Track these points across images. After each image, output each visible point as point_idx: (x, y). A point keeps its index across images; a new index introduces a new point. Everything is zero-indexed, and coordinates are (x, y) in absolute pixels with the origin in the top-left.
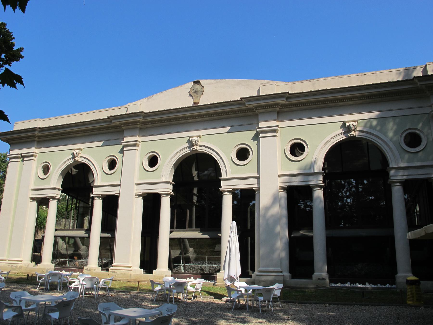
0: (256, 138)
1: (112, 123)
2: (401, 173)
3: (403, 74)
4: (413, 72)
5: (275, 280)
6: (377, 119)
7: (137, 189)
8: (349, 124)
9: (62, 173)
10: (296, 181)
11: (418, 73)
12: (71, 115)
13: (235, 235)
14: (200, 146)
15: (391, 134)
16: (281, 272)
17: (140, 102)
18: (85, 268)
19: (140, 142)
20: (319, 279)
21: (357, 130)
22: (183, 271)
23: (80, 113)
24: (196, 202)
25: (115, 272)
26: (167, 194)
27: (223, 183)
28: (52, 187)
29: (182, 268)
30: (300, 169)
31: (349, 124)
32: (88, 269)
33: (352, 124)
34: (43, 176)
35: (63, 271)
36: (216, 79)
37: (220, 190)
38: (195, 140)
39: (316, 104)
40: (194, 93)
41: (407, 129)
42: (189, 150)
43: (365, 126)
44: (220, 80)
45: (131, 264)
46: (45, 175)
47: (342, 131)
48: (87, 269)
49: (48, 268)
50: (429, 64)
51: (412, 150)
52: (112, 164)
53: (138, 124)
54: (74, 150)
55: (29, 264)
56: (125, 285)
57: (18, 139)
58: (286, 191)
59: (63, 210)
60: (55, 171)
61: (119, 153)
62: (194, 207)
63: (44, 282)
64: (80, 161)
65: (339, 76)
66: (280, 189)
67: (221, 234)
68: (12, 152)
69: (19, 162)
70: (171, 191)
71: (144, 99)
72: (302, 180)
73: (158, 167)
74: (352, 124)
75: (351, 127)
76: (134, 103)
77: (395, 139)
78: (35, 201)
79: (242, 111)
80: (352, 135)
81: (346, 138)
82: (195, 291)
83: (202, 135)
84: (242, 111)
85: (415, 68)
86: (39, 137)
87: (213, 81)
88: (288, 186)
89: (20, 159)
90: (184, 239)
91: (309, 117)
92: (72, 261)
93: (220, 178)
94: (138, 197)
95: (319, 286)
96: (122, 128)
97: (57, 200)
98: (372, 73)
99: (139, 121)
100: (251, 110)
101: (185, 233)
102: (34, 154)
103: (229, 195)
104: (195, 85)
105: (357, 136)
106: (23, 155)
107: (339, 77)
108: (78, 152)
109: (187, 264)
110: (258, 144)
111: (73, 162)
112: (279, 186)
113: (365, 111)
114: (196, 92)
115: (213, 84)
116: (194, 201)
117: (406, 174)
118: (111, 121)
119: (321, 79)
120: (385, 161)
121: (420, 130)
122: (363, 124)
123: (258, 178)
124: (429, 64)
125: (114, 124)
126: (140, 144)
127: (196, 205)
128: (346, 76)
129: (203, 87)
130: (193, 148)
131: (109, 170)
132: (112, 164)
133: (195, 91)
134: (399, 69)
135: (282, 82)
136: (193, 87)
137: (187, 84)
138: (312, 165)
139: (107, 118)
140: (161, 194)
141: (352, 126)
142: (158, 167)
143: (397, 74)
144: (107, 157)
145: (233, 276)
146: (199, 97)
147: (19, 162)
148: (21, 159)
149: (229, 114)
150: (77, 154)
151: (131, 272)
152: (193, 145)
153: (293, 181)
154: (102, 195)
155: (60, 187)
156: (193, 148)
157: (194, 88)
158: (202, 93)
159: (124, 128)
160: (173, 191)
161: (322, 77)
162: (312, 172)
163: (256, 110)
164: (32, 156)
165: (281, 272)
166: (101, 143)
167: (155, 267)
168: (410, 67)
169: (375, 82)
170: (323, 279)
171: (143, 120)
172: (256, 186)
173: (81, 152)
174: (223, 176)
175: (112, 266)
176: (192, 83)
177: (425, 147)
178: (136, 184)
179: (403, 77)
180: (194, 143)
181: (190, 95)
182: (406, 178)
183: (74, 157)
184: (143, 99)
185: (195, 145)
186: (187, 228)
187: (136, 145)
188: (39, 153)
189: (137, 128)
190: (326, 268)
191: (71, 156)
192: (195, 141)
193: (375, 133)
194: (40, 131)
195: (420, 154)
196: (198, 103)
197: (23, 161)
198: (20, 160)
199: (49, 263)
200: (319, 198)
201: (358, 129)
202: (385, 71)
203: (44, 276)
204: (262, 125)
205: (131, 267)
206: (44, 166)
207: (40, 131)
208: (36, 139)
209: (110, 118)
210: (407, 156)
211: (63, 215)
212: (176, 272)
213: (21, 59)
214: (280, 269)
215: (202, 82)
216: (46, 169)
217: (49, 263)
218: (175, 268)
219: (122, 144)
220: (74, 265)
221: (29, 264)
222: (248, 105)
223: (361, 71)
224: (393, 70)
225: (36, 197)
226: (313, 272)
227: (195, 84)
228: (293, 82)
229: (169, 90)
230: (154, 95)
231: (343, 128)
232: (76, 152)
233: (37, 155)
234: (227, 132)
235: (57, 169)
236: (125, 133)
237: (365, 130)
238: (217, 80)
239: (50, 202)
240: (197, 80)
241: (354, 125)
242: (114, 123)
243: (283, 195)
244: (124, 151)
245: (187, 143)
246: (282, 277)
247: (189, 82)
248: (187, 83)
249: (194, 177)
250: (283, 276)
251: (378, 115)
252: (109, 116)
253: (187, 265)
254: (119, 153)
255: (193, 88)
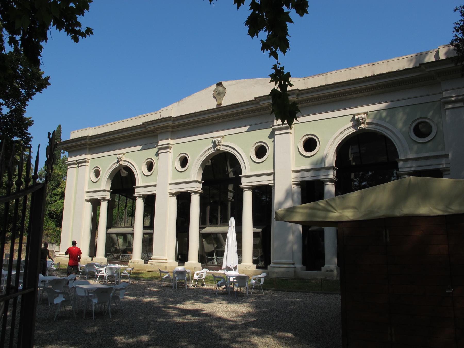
0: (272, 136)
1: (147, 128)
2: (409, 164)
3: (414, 61)
4: (425, 57)
5: (286, 271)
6: (386, 110)
7: (170, 189)
8: (358, 117)
9: (110, 176)
10: (308, 176)
11: (431, 58)
12: (115, 122)
13: (233, 229)
14: (124, 161)
15: (400, 125)
16: (293, 264)
17: (171, 107)
18: (130, 261)
19: (172, 145)
20: (327, 271)
21: (366, 122)
22: (216, 263)
23: (123, 120)
24: (232, 198)
25: (153, 264)
26: (196, 193)
27: (243, 180)
28: (102, 189)
29: (215, 261)
30: (312, 164)
31: (358, 117)
32: (133, 262)
33: (361, 117)
34: (180, 169)
35: (117, 264)
36: (236, 79)
37: (240, 187)
38: (218, 141)
39: (331, 97)
40: (219, 95)
41: (416, 118)
42: (214, 150)
43: (374, 118)
44: (240, 80)
45: (166, 257)
46: (97, 178)
47: (353, 124)
48: (131, 262)
49: (102, 261)
50: (441, 47)
51: (421, 140)
52: (150, 166)
53: (169, 128)
54: (118, 154)
55: (87, 258)
56: (149, 276)
57: (115, 140)
58: (299, 186)
59: (129, 209)
60: (104, 175)
61: (155, 155)
62: (230, 203)
63: (84, 272)
64: (124, 164)
65: (350, 68)
66: (293, 184)
67: (153, 231)
68: (70, 159)
69: (76, 167)
70: (201, 190)
71: (175, 103)
72: (313, 175)
73: (318, 151)
74: (361, 117)
75: (360, 120)
76: (166, 108)
77: (404, 129)
78: (141, 198)
79: (248, 112)
80: (361, 128)
81: (356, 131)
82: (198, 279)
83: (225, 135)
84: (248, 112)
85: (428, 52)
86: (90, 144)
87: (233, 82)
88: (301, 181)
89: (76, 165)
90: (218, 234)
91: (322, 112)
92: (126, 255)
93: (240, 176)
94: (171, 196)
95: (327, 277)
96: (156, 132)
97: (107, 201)
98: (383, 61)
99: (170, 125)
100: (153, 131)
101: (216, 228)
102: (86, 160)
103: (248, 191)
104: (217, 87)
105: (366, 129)
106: (78, 161)
107: (350, 68)
108: (220, 140)
109: (256, 259)
110: (274, 141)
111: (118, 166)
112: (292, 182)
113: (380, 102)
114: (219, 94)
115: (234, 85)
116: (229, 197)
117: (414, 165)
118: (146, 127)
119: (333, 72)
120: (396, 153)
121: (430, 119)
122: (372, 116)
123: (273, 174)
124: (441, 47)
125: (262, 105)
126: (172, 146)
127: (231, 202)
128: (358, 67)
129: (225, 88)
130: (216, 148)
131: (181, 168)
132: (150, 166)
133: (218, 93)
134: (411, 55)
135: (296, 78)
136: (216, 90)
137: (211, 86)
138: (323, 160)
139: (142, 124)
140: (191, 192)
141: (360, 118)
142: (266, 158)
143: (408, 61)
144: (179, 155)
145: (229, 266)
146: (222, 99)
147: (76, 167)
148: (77, 165)
149: (320, 99)
150: (120, 158)
151: (167, 265)
152: (217, 146)
153: (305, 176)
154: (252, 186)
155: (109, 189)
156: (216, 148)
157: (217, 89)
158: (224, 95)
159: (157, 132)
160: (202, 190)
161: (334, 70)
162: (323, 166)
163: (270, 108)
164: (85, 162)
165: (293, 264)
166: (140, 147)
167: (187, 260)
168: (422, 52)
169: (352, 79)
170: (332, 271)
171: (297, 99)
172: (272, 182)
173: (124, 156)
174: (243, 174)
175: (151, 259)
176: (215, 85)
177: (434, 137)
178: (86, 192)
179: (415, 64)
180: (217, 143)
181: (214, 97)
182: (414, 170)
183: (118, 161)
184: (174, 104)
185: (361, 124)
186: (219, 224)
187: (168, 147)
188: (91, 159)
189: (169, 131)
190: (336, 260)
191: (117, 160)
192: (217, 142)
193: (384, 125)
194: (89, 139)
195: (429, 144)
196: (221, 104)
197: (78, 167)
198: (76, 166)
199: (87, 256)
200: (329, 192)
201: (367, 121)
202: (396, 59)
203: (84, 266)
204: (160, 143)
205: (166, 260)
206: (95, 170)
207: (89, 139)
208: (88, 146)
209: (144, 124)
210: (415, 147)
211: (130, 213)
212: (212, 264)
213: (48, 86)
214: (292, 261)
215: (224, 83)
216: (97, 173)
217: (87, 256)
218: (211, 261)
219: (157, 147)
220: (127, 259)
221: (87, 258)
222: (262, 104)
223: (372, 61)
224: (404, 57)
225: (175, 192)
226: (323, 265)
227: (218, 86)
228: (306, 77)
229: (196, 94)
230: (184, 99)
231: (353, 121)
232: (120, 156)
233: (90, 160)
234: (246, 131)
235: (105, 173)
236: (159, 137)
237: (374, 122)
238: (238, 81)
239: (101, 203)
240: (220, 82)
241: (362, 118)
242: (262, 105)
243: (296, 189)
244: (159, 154)
245: (212, 143)
246: (293, 269)
247: (212, 84)
248: (211, 85)
249: (228, 174)
250: (295, 267)
251: (387, 106)
252: (143, 122)
253: (222, 258)
254: (155, 155)
255: (216, 91)
